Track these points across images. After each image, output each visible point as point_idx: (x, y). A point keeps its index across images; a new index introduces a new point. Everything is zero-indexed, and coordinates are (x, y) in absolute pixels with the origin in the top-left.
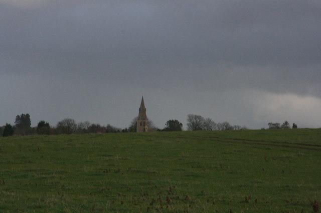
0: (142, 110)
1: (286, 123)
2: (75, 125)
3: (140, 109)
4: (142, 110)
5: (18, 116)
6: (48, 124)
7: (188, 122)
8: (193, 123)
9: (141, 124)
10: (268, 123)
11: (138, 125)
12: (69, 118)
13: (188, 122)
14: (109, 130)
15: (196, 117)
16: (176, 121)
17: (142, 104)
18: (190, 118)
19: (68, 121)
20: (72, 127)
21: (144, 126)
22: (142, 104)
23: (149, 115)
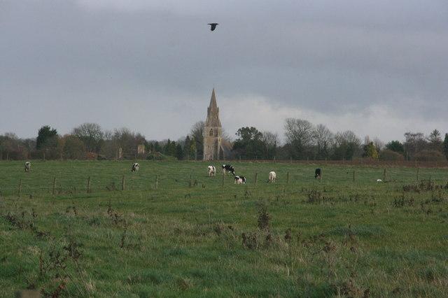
0: (213, 111)
1: (436, 133)
2: (101, 134)
3: (209, 110)
4: (213, 111)
5: (321, 125)
6: (54, 132)
7: (287, 131)
8: (296, 140)
9: (211, 134)
10: (404, 133)
11: (206, 134)
12: (91, 121)
13: (287, 131)
14: (129, 145)
15: (300, 123)
16: (253, 130)
17: (213, 101)
18: (290, 124)
19: (89, 127)
20: (96, 136)
21: (217, 136)
22: (213, 101)
23: (224, 117)
